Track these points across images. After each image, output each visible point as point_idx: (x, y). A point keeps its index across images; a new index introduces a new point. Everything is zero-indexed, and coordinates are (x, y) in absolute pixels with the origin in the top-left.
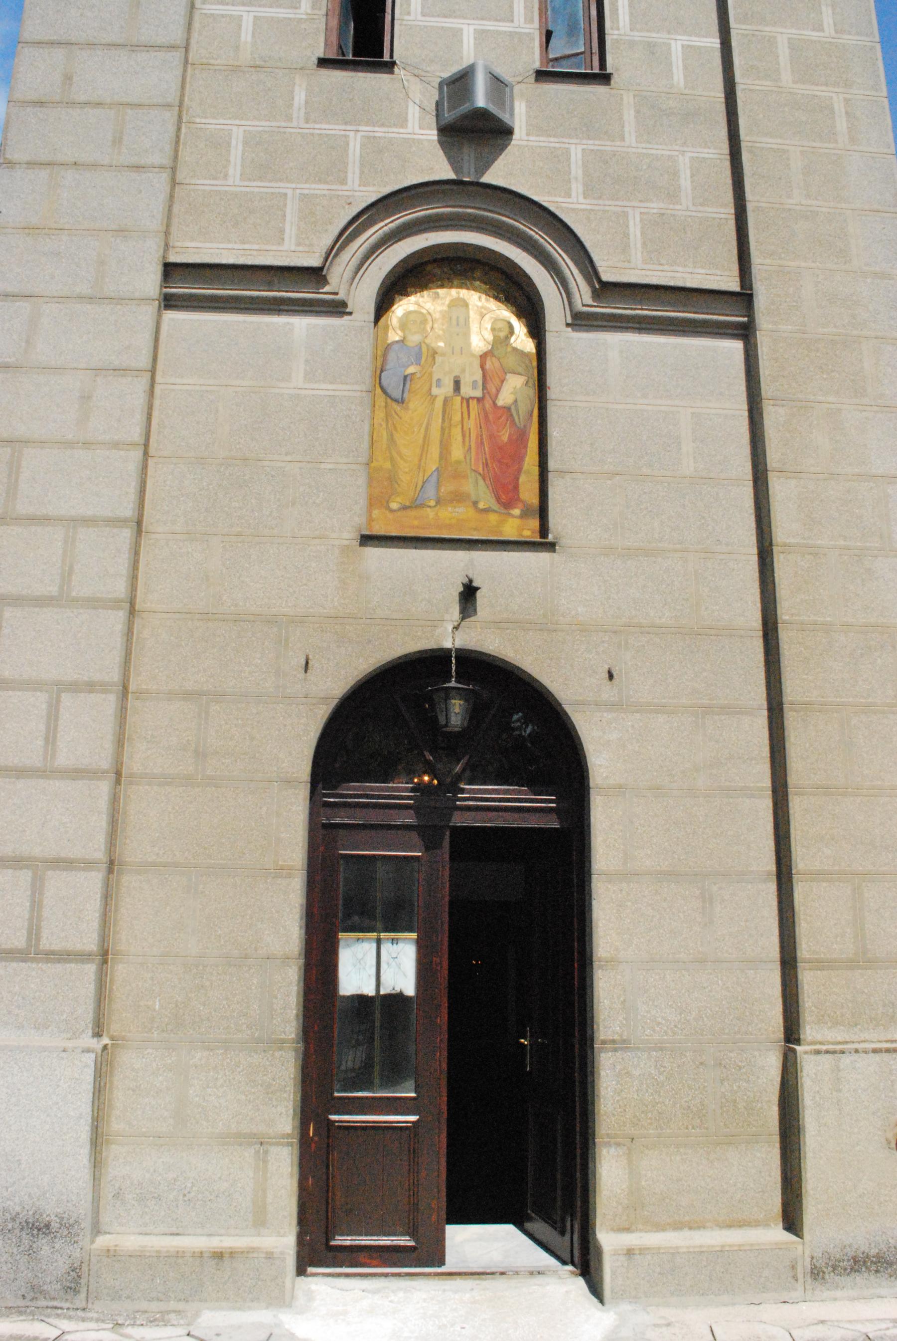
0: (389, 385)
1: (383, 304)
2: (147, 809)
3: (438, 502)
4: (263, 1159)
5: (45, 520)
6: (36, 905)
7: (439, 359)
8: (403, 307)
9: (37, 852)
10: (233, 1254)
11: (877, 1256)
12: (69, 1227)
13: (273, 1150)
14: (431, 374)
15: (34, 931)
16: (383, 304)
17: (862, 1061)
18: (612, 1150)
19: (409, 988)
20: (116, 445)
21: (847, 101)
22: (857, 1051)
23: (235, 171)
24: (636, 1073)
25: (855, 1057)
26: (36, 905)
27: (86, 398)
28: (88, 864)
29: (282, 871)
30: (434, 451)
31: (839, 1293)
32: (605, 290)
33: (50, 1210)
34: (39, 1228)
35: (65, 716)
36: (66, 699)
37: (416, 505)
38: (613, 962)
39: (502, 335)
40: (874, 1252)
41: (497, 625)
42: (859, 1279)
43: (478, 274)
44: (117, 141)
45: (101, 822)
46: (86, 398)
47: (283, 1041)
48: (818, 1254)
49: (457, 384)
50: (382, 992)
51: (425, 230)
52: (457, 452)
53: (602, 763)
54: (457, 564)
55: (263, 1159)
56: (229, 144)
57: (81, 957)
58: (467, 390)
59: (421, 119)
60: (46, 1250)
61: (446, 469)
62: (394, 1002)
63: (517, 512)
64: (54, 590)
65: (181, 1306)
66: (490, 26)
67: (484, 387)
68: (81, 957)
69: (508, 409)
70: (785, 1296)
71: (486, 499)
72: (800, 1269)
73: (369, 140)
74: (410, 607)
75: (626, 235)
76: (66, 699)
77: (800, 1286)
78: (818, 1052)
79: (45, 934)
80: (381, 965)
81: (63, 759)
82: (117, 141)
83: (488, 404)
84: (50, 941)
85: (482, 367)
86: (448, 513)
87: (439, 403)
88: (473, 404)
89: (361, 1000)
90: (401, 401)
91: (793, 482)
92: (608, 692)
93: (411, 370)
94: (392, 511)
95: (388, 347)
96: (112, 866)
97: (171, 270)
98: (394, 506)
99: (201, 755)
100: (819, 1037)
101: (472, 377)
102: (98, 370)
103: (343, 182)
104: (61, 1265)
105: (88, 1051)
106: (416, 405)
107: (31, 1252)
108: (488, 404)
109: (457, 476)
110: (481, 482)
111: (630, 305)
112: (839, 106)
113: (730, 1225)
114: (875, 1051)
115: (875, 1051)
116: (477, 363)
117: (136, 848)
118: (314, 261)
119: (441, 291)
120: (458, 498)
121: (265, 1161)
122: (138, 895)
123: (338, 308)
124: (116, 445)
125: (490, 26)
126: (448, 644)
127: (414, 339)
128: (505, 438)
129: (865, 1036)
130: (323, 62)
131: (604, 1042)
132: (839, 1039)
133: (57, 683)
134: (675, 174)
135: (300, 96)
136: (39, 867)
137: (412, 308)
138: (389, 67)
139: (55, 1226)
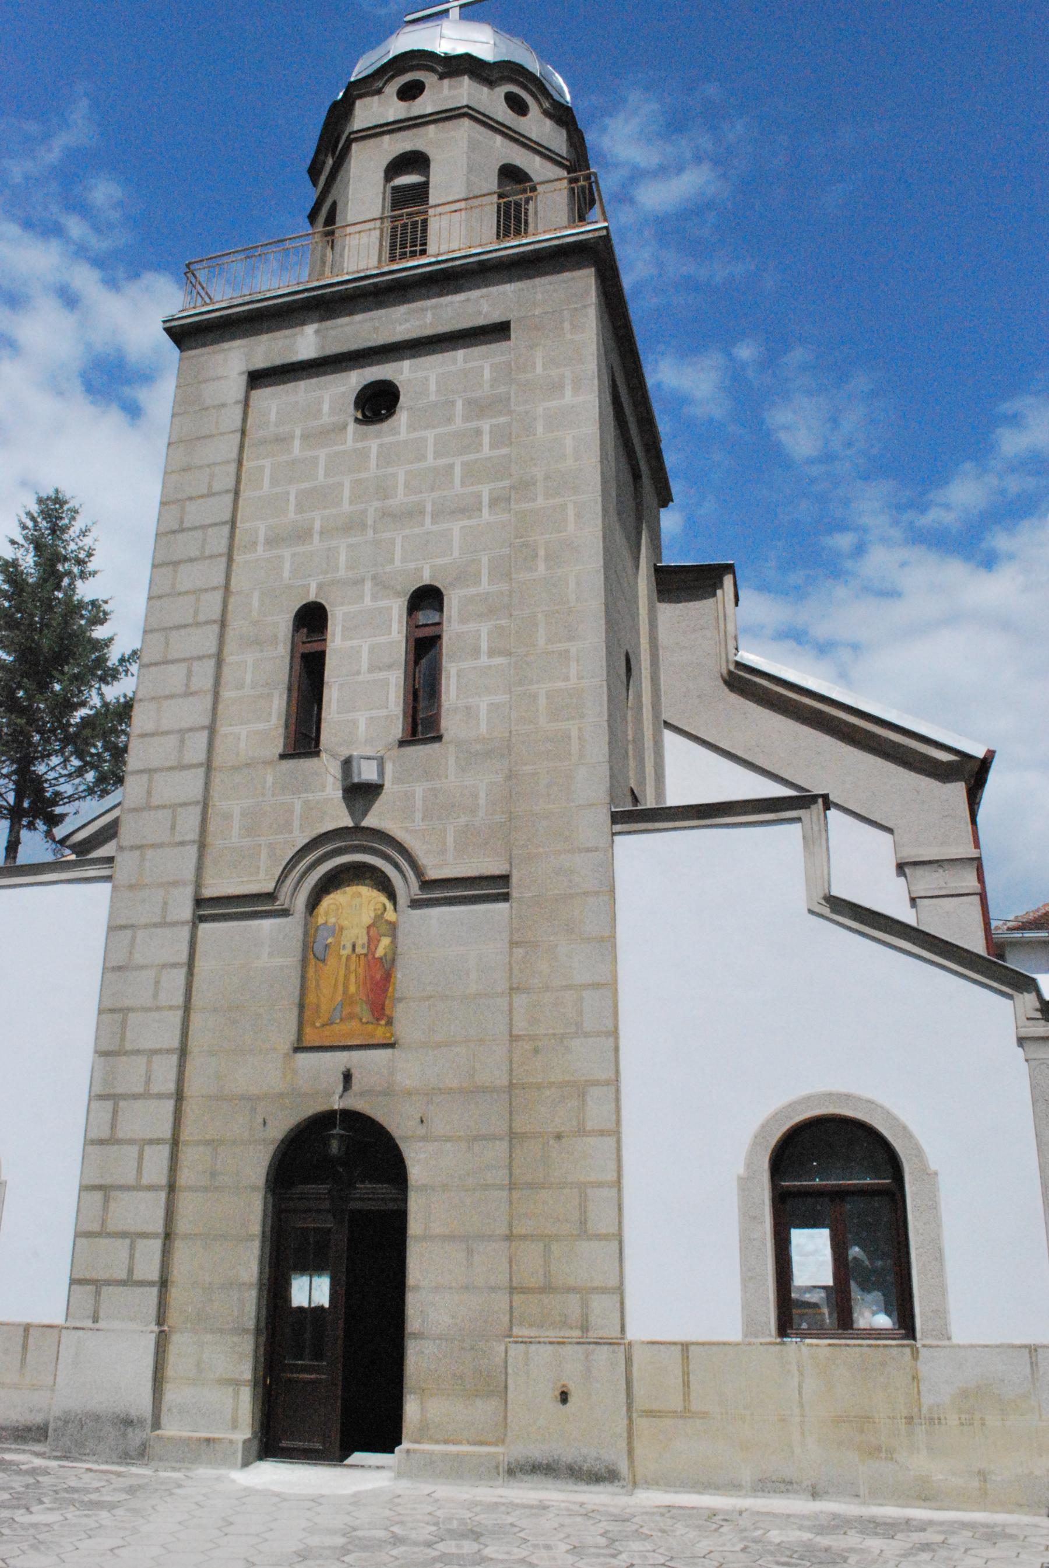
0: (312, 952)
1: (313, 904)
2: (188, 1204)
3: (341, 1020)
4: (237, 1393)
5: (137, 1052)
6: (132, 1257)
7: (345, 932)
8: (328, 902)
9: (132, 1229)
10: (214, 1439)
11: (547, 1465)
12: (142, 1423)
13: (242, 1388)
14: (340, 942)
15: (130, 1271)
16: (313, 904)
17: (541, 1348)
18: (412, 1396)
19: (327, 1305)
20: (171, 1008)
21: (580, 729)
22: (539, 1342)
23: (235, 832)
24: (427, 1352)
25: (538, 1346)
26: (132, 1257)
27: (157, 983)
28: (155, 1236)
29: (250, 1238)
30: (341, 988)
31: (523, 1485)
32: (427, 884)
33: (134, 1414)
34: (128, 1422)
35: (146, 1157)
36: (146, 1147)
37: (330, 1023)
38: (417, 1288)
39: (379, 912)
40: (545, 1462)
41: (362, 1094)
42: (536, 1478)
43: (368, 875)
44: (173, 827)
45: (161, 1213)
46: (157, 983)
47: (248, 1330)
48: (512, 1460)
49: (354, 946)
50: (313, 1305)
51: (332, 857)
52: (352, 989)
53: (416, 1173)
54: (340, 1060)
55: (237, 1393)
56: (232, 816)
57: (151, 1284)
58: (359, 950)
59: (334, 784)
60: (130, 1435)
61: (349, 999)
62: (318, 1311)
63: (383, 1022)
64: (141, 1090)
65: (189, 1466)
66: (375, 713)
67: (368, 947)
68: (151, 1284)
69: (381, 959)
70: (491, 1484)
71: (366, 1016)
72: (501, 1469)
73: (306, 802)
74: (316, 1084)
75: (445, 844)
76: (146, 1147)
77: (500, 1479)
78: (516, 1342)
79: (135, 1272)
80: (310, 1291)
81: (145, 1181)
82: (173, 827)
83: (370, 957)
84: (138, 1276)
85: (368, 933)
86: (345, 1027)
87: (344, 959)
88: (362, 957)
89: (301, 1309)
90: (324, 961)
91: (524, 996)
92: (421, 1131)
93: (330, 940)
94: (317, 1028)
95: (317, 929)
96: (168, 1236)
97: (199, 902)
98: (318, 1024)
99: (213, 1175)
100: (520, 1334)
101: (363, 939)
102: (164, 966)
103: (291, 832)
104: (138, 1442)
105: (152, 1332)
106: (332, 961)
107: (124, 1435)
108: (370, 957)
109: (352, 1003)
110: (364, 1006)
111: (441, 891)
112: (574, 734)
113: (475, 1444)
114: (551, 1343)
115: (551, 1343)
116: (365, 932)
117: (182, 1226)
118: (269, 887)
119: (347, 889)
120: (351, 1016)
121: (238, 1394)
122: (181, 1250)
123: (285, 913)
124: (171, 1008)
125: (375, 713)
126: (336, 1107)
127: (332, 920)
128: (378, 977)
129: (547, 1334)
130: (283, 757)
131: (410, 1334)
132: (532, 1335)
133: (144, 1140)
134: (476, 796)
135: (270, 779)
136: (133, 1237)
137: (331, 901)
138: (438, 738)
139: (135, 1421)
